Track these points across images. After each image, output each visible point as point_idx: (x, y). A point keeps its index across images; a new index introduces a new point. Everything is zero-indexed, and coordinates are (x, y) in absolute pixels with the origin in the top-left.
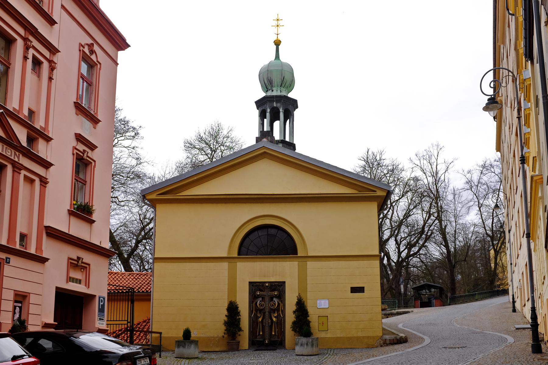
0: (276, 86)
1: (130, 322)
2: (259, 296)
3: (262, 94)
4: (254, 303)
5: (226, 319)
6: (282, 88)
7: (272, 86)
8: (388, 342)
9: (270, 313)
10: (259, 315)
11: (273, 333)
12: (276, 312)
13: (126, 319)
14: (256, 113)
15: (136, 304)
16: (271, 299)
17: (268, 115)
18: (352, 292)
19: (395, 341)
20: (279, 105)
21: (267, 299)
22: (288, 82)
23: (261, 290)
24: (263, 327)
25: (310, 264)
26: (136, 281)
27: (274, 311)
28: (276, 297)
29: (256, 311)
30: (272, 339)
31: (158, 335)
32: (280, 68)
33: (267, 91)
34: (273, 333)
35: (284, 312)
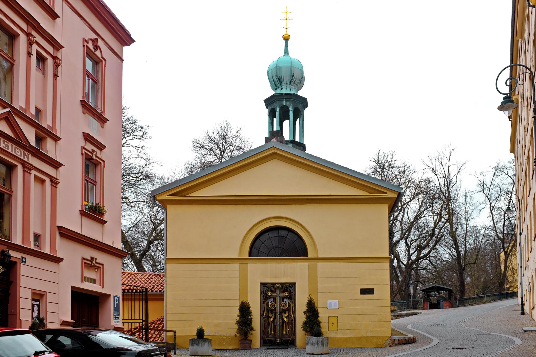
1: (145, 321)
2: (270, 297)
3: (271, 92)
4: (266, 303)
7: (281, 84)
8: (397, 342)
9: (281, 313)
10: (270, 315)
11: (284, 333)
12: (287, 312)
13: (141, 318)
16: (283, 299)
17: (277, 114)
18: (361, 294)
20: (288, 103)
21: (278, 300)
22: (298, 80)
23: (272, 291)
24: (275, 327)
25: (321, 266)
27: (285, 311)
28: (287, 297)
30: (284, 339)
31: (172, 334)
32: (289, 65)
33: (276, 89)
34: (284, 333)
35: (294, 312)
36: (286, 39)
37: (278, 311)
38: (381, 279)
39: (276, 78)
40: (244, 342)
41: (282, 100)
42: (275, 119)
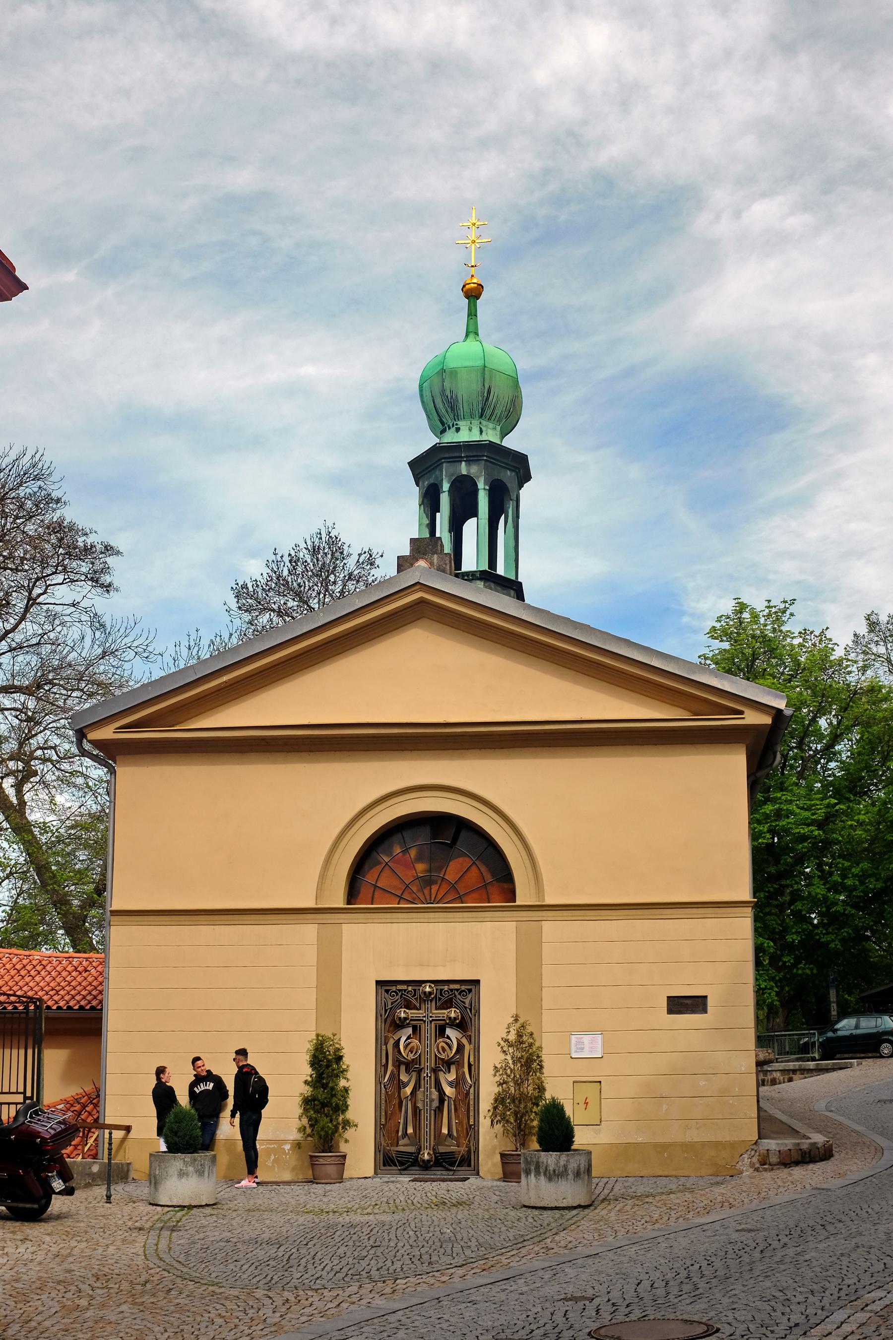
0: (467, 415)
1: (31, 1098)
2: (400, 1025)
3: (429, 441)
5: (307, 1090)
6: (484, 423)
8: (774, 1159)
9: (435, 1071)
10: (404, 1077)
11: (445, 1131)
13: (21, 1090)
14: (413, 493)
16: (441, 1031)
17: (445, 500)
18: (670, 1011)
19: (796, 1156)
21: (428, 1030)
22: (500, 403)
23: (409, 1006)
25: (552, 929)
26: (79, 979)
29: (398, 1063)
30: (442, 1149)
32: (479, 363)
33: (443, 431)
34: (445, 1131)
36: (473, 294)
37: (428, 1064)
38: (725, 956)
39: (442, 400)
41: (459, 460)
42: (438, 514)
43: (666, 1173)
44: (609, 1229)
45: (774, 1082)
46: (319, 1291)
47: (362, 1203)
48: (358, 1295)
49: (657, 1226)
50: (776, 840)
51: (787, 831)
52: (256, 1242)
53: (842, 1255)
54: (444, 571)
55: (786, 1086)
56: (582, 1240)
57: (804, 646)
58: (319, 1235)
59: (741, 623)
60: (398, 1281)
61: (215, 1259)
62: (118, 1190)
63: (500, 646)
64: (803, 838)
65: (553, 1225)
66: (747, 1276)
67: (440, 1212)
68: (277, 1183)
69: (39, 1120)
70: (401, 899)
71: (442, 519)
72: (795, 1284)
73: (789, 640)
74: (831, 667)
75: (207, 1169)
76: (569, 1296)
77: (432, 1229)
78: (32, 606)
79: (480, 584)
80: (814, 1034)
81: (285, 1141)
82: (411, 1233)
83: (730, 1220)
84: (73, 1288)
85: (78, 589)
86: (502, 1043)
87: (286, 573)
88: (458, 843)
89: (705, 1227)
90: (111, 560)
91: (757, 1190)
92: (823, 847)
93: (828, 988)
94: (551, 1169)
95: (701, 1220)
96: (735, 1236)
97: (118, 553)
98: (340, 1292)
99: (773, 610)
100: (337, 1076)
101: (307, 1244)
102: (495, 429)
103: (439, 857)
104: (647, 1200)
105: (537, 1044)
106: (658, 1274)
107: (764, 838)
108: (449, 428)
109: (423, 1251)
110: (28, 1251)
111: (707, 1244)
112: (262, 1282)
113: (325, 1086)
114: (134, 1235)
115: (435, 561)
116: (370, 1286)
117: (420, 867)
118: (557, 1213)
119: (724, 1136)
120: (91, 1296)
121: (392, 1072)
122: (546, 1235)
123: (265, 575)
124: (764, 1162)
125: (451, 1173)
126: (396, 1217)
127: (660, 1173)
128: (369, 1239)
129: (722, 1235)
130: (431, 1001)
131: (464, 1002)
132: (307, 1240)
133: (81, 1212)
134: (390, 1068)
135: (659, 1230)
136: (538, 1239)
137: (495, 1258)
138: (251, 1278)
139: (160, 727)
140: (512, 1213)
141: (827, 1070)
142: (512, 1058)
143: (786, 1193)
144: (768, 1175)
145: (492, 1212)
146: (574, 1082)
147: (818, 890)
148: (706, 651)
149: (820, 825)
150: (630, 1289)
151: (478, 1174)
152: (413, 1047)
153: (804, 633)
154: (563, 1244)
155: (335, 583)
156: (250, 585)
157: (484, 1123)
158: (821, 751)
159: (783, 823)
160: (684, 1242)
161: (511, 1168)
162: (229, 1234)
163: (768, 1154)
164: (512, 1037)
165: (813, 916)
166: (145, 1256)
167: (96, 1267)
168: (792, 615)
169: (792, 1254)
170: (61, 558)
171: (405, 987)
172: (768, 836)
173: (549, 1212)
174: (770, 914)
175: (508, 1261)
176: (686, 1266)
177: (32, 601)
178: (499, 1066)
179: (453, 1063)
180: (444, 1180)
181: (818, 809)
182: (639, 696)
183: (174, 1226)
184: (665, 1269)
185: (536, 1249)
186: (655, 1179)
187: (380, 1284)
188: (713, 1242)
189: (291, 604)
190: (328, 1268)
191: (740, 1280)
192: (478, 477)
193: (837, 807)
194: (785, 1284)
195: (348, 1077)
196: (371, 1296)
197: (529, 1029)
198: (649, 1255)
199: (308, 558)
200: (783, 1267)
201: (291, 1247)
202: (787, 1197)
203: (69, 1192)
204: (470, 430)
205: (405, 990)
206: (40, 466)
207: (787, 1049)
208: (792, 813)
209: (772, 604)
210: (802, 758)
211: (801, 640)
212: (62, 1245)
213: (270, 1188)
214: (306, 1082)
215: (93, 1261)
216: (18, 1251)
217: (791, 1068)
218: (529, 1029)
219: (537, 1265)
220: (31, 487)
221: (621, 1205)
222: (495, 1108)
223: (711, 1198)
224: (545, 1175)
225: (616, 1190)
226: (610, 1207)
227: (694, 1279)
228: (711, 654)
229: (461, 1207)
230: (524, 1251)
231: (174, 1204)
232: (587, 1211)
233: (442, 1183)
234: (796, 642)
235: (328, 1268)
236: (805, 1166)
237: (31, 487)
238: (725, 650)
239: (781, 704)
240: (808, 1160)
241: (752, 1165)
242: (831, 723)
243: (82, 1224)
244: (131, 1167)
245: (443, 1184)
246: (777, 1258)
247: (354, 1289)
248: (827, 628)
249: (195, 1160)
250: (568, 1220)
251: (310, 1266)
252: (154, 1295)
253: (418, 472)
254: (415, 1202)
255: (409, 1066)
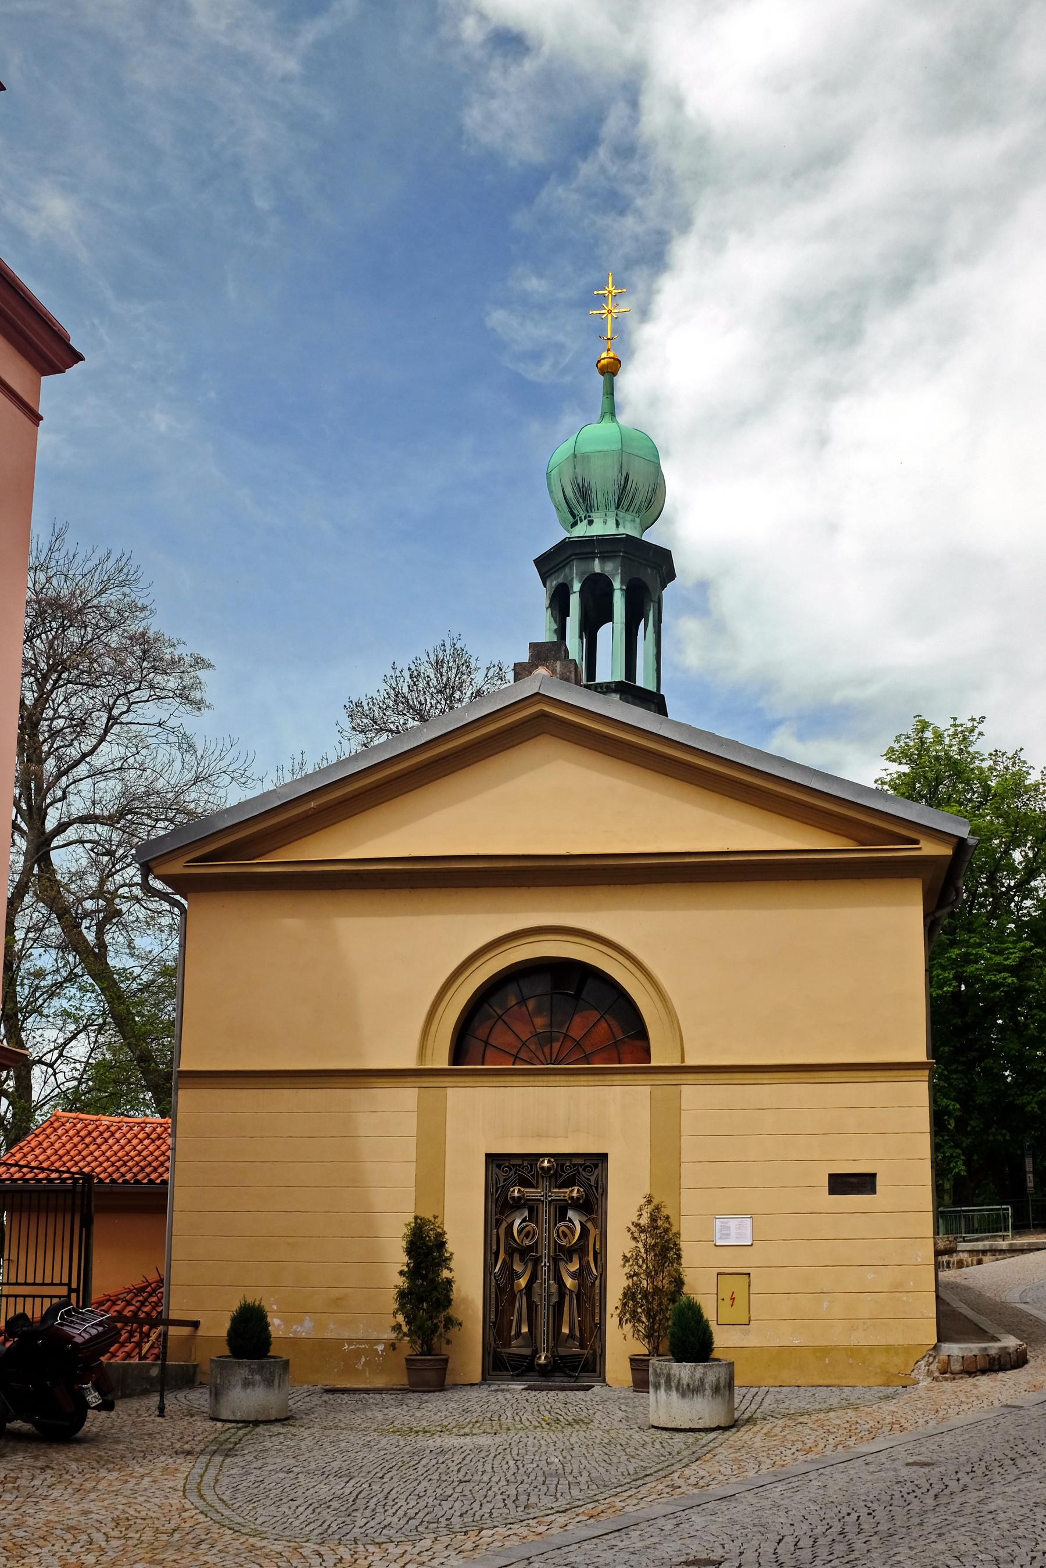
1: (77, 1291)
2: (518, 1204)
3: (558, 534)
4: (504, 1225)
6: (621, 514)
7: (589, 508)
8: (956, 1367)
9: (556, 1261)
10: (518, 1268)
11: (565, 1330)
12: (576, 1259)
13: (65, 1280)
14: (539, 594)
15: (101, 1225)
16: (562, 1215)
17: (575, 601)
18: (833, 1191)
19: (982, 1363)
20: (609, 568)
21: (545, 1213)
23: (525, 1183)
24: (532, 1307)
25: (694, 1094)
27: (569, 1253)
29: (510, 1252)
30: (562, 1351)
31: (186, 1331)
34: (565, 1330)
35: (600, 1256)
38: (898, 1130)
40: (419, 1366)
41: (590, 557)
43: (828, 1382)
44: (752, 1460)
45: (960, 1264)
46: (383, 1546)
47: (462, 1419)
48: (429, 1553)
49: (810, 1456)
50: (963, 988)
51: (978, 979)
52: (323, 1473)
53: (1036, 1504)
54: (568, 680)
55: (974, 1269)
56: (717, 1475)
57: (995, 769)
58: (400, 1464)
59: (923, 743)
60: (483, 1533)
61: (267, 1497)
62: (176, 1400)
63: (776, 816)
64: (995, 986)
65: (685, 1453)
66: (915, 1532)
67: (551, 1433)
68: (367, 1391)
69: (72, 1322)
70: (516, 1059)
71: (573, 623)
72: (975, 1548)
73: (977, 763)
74: (1026, 793)
75: (277, 1378)
76: (692, 1558)
77: (537, 1458)
78: (112, 726)
79: (616, 697)
80: (1007, 1209)
81: (378, 1341)
82: (511, 1463)
83: (899, 1448)
84: (84, 1537)
85: (166, 706)
86: (633, 1229)
87: (406, 690)
88: (584, 993)
89: (869, 1459)
90: (203, 674)
91: (935, 1407)
92: (1018, 994)
93: (1023, 1156)
94: (685, 1382)
95: (865, 1448)
96: (904, 1472)
97: (210, 666)
98: (409, 1548)
99: (960, 729)
100: (439, 1265)
101: (382, 1478)
102: (634, 521)
103: (557, 1013)
104: (801, 1419)
105: (674, 1230)
106: (805, 1527)
107: (950, 986)
108: (581, 521)
109: (521, 1489)
110: (46, 1483)
111: (869, 1484)
112: (316, 1532)
113: (424, 1278)
114: (178, 1461)
115: (558, 669)
116: (446, 1540)
117: (540, 1022)
118: (691, 1437)
119: (896, 1338)
120: (102, 1549)
121: (504, 1261)
122: (674, 1468)
123: (382, 692)
124: (946, 1371)
125: (573, 1380)
126: (498, 1439)
127: (821, 1382)
128: (459, 1470)
129: (888, 1470)
130: (550, 1177)
131: (589, 1180)
132: (384, 1471)
133: (125, 1429)
134: (502, 1256)
135: (813, 1461)
136: (662, 1473)
137: (607, 1501)
138: (303, 1525)
139: (231, 860)
140: (636, 1436)
141: (1022, 1251)
142: (645, 1245)
143: (970, 1412)
144: (948, 1386)
145: (613, 1433)
146: (718, 1274)
147: (1012, 1046)
148: (883, 774)
149: (1013, 971)
150: (768, 1548)
151: (604, 1381)
152: (528, 1233)
153: (995, 754)
154: (693, 1481)
155: (460, 700)
156: (365, 704)
157: (612, 1323)
158: (1015, 887)
159: (971, 969)
160: (841, 1479)
161: (641, 1377)
162: (293, 1461)
163: (949, 1360)
164: (644, 1221)
165: (1007, 1073)
166: (184, 1491)
167: (120, 1507)
168: (981, 734)
169: (972, 1502)
170: (144, 673)
171: (519, 1162)
172: (955, 984)
173: (682, 1435)
174: (955, 1071)
175: (623, 1504)
176: (841, 1515)
177: (113, 720)
178: (629, 1255)
179: (575, 1251)
180: (563, 1389)
181: (1012, 954)
182: (797, 823)
183: (230, 1450)
184: (814, 1519)
185: (660, 1487)
186: (813, 1390)
187: (460, 1537)
188: (877, 1481)
189: (411, 723)
190: (401, 1513)
191: (907, 1539)
192: (614, 575)
193: (1034, 951)
194: (963, 1548)
195: (452, 1266)
196: (446, 1553)
197: (665, 1212)
198: (797, 1497)
199: (431, 673)
200: (962, 1520)
201: (363, 1480)
202: (970, 1417)
203: (107, 1406)
204: (605, 523)
205: (520, 1165)
206: (125, 571)
207: (976, 1225)
208: (982, 957)
209: (958, 722)
210: (993, 896)
211: (991, 763)
212: (87, 1476)
213: (357, 1396)
214: (401, 1273)
215: (120, 1498)
216: (32, 1484)
217: (981, 1248)
218: (665, 1212)
219: (659, 1510)
220: (113, 595)
221: (769, 1426)
222: (624, 1305)
223: (879, 1418)
224: (677, 1390)
225: (765, 1404)
226: (755, 1429)
227: (850, 1536)
228: (889, 778)
229: (577, 1427)
230: (644, 1490)
231: (237, 1418)
232: (728, 1433)
233: (559, 1393)
234: (986, 765)
235: (401, 1513)
236: (993, 1375)
237: (113, 595)
238: (904, 774)
239: (963, 832)
240: (997, 1367)
241: (929, 1373)
242: (1026, 855)
243: (121, 1446)
244: (198, 1370)
245: (562, 1395)
246: (954, 1508)
247: (427, 1543)
248: (1022, 749)
249: (263, 1367)
250: (704, 1446)
251: (380, 1509)
252: (179, 1550)
253: (544, 571)
254: (524, 1418)
255: (524, 1253)
